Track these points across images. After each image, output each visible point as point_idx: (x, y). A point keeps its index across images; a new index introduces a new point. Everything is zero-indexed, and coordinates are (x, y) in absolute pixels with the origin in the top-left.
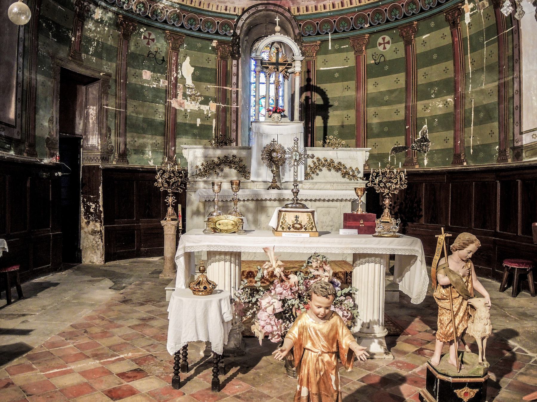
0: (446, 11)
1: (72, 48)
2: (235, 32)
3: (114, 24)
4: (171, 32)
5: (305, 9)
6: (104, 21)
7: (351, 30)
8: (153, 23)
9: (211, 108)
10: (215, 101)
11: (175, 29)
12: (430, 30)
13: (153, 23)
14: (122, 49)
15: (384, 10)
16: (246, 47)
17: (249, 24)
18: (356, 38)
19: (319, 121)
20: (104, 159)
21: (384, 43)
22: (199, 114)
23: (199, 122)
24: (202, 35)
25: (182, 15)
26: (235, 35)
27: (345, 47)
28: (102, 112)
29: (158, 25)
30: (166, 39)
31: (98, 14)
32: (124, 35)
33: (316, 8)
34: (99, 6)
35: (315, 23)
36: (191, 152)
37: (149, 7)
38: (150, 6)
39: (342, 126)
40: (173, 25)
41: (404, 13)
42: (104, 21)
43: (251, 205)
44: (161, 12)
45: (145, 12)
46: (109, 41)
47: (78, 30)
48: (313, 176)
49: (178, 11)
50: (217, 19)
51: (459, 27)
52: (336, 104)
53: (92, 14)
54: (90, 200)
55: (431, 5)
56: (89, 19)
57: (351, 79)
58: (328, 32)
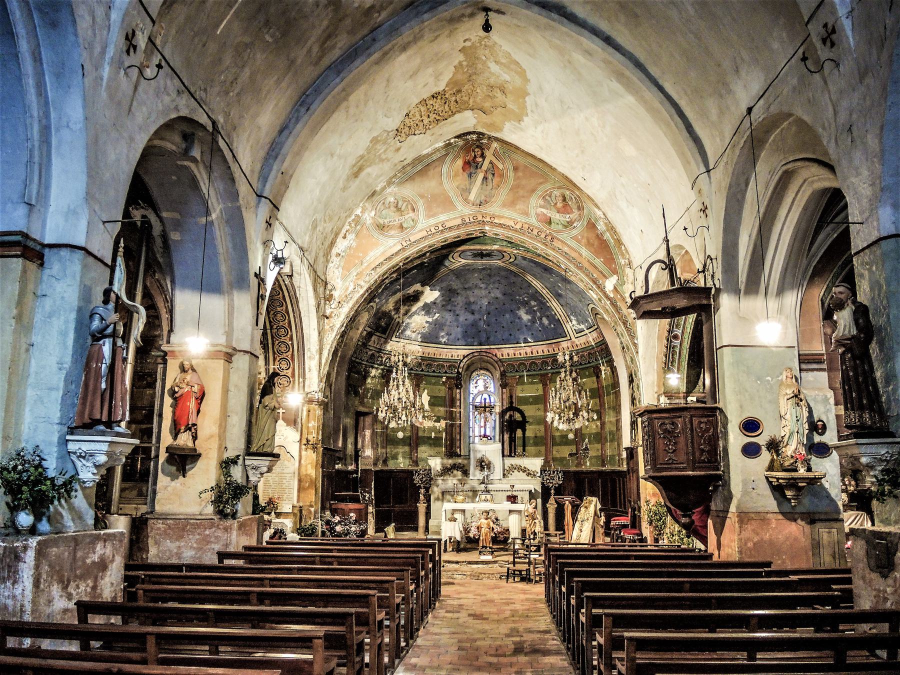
2: (458, 371)
9: (442, 424)
10: (445, 419)
18: (542, 375)
19: (519, 433)
20: (375, 464)
22: (434, 429)
23: (433, 435)
28: (374, 434)
31: (373, 372)
33: (514, 355)
36: (434, 461)
39: (536, 437)
43: (405, 225)
48: (509, 475)
52: (531, 420)
54: (365, 492)
57: (541, 404)
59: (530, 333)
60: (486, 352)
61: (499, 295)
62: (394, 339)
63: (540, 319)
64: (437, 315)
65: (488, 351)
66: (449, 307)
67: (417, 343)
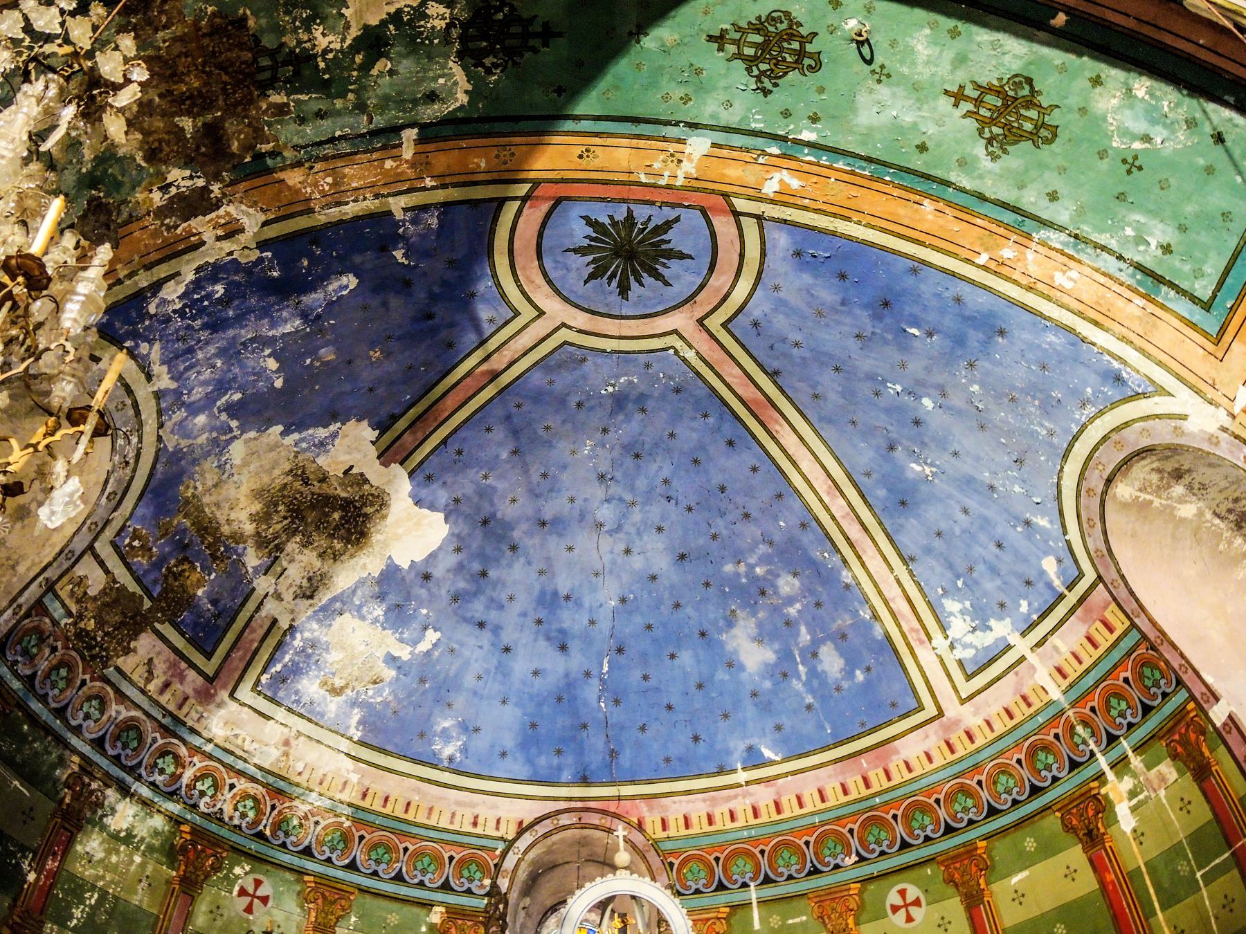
0: (1059, 806)
1: (19, 903)
2: (494, 885)
3: (161, 849)
4: (318, 880)
5: (681, 822)
6: (135, 836)
7: (810, 874)
8: (271, 852)
11: (331, 872)
12: (1027, 861)
13: (271, 852)
14: (170, 921)
15: (889, 817)
16: (523, 926)
17: (534, 863)
21: (906, 906)
24: (403, 891)
25: (357, 835)
26: (494, 892)
27: (797, 920)
29: (286, 858)
30: (303, 898)
31: (124, 816)
32: (184, 880)
33: (711, 820)
34: (132, 796)
35: (711, 858)
37: (269, 809)
38: (273, 808)
40: (329, 860)
41: (946, 822)
42: (135, 836)
44: (301, 825)
45: (256, 822)
46: (136, 893)
47: (55, 854)
49: (347, 824)
50: (448, 847)
51: (1107, 845)
53: (106, 816)
55: (1015, 795)
56: (94, 827)
58: (747, 880)
59: (770, 724)
60: (603, 812)
61: (662, 563)
62: (245, 692)
63: (812, 654)
64: (432, 636)
65: (612, 807)
66: (478, 608)
67: (345, 745)
